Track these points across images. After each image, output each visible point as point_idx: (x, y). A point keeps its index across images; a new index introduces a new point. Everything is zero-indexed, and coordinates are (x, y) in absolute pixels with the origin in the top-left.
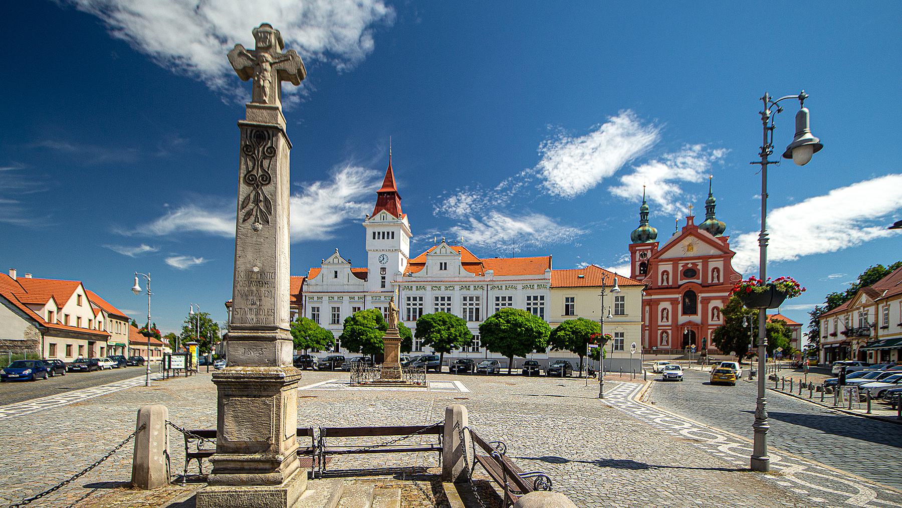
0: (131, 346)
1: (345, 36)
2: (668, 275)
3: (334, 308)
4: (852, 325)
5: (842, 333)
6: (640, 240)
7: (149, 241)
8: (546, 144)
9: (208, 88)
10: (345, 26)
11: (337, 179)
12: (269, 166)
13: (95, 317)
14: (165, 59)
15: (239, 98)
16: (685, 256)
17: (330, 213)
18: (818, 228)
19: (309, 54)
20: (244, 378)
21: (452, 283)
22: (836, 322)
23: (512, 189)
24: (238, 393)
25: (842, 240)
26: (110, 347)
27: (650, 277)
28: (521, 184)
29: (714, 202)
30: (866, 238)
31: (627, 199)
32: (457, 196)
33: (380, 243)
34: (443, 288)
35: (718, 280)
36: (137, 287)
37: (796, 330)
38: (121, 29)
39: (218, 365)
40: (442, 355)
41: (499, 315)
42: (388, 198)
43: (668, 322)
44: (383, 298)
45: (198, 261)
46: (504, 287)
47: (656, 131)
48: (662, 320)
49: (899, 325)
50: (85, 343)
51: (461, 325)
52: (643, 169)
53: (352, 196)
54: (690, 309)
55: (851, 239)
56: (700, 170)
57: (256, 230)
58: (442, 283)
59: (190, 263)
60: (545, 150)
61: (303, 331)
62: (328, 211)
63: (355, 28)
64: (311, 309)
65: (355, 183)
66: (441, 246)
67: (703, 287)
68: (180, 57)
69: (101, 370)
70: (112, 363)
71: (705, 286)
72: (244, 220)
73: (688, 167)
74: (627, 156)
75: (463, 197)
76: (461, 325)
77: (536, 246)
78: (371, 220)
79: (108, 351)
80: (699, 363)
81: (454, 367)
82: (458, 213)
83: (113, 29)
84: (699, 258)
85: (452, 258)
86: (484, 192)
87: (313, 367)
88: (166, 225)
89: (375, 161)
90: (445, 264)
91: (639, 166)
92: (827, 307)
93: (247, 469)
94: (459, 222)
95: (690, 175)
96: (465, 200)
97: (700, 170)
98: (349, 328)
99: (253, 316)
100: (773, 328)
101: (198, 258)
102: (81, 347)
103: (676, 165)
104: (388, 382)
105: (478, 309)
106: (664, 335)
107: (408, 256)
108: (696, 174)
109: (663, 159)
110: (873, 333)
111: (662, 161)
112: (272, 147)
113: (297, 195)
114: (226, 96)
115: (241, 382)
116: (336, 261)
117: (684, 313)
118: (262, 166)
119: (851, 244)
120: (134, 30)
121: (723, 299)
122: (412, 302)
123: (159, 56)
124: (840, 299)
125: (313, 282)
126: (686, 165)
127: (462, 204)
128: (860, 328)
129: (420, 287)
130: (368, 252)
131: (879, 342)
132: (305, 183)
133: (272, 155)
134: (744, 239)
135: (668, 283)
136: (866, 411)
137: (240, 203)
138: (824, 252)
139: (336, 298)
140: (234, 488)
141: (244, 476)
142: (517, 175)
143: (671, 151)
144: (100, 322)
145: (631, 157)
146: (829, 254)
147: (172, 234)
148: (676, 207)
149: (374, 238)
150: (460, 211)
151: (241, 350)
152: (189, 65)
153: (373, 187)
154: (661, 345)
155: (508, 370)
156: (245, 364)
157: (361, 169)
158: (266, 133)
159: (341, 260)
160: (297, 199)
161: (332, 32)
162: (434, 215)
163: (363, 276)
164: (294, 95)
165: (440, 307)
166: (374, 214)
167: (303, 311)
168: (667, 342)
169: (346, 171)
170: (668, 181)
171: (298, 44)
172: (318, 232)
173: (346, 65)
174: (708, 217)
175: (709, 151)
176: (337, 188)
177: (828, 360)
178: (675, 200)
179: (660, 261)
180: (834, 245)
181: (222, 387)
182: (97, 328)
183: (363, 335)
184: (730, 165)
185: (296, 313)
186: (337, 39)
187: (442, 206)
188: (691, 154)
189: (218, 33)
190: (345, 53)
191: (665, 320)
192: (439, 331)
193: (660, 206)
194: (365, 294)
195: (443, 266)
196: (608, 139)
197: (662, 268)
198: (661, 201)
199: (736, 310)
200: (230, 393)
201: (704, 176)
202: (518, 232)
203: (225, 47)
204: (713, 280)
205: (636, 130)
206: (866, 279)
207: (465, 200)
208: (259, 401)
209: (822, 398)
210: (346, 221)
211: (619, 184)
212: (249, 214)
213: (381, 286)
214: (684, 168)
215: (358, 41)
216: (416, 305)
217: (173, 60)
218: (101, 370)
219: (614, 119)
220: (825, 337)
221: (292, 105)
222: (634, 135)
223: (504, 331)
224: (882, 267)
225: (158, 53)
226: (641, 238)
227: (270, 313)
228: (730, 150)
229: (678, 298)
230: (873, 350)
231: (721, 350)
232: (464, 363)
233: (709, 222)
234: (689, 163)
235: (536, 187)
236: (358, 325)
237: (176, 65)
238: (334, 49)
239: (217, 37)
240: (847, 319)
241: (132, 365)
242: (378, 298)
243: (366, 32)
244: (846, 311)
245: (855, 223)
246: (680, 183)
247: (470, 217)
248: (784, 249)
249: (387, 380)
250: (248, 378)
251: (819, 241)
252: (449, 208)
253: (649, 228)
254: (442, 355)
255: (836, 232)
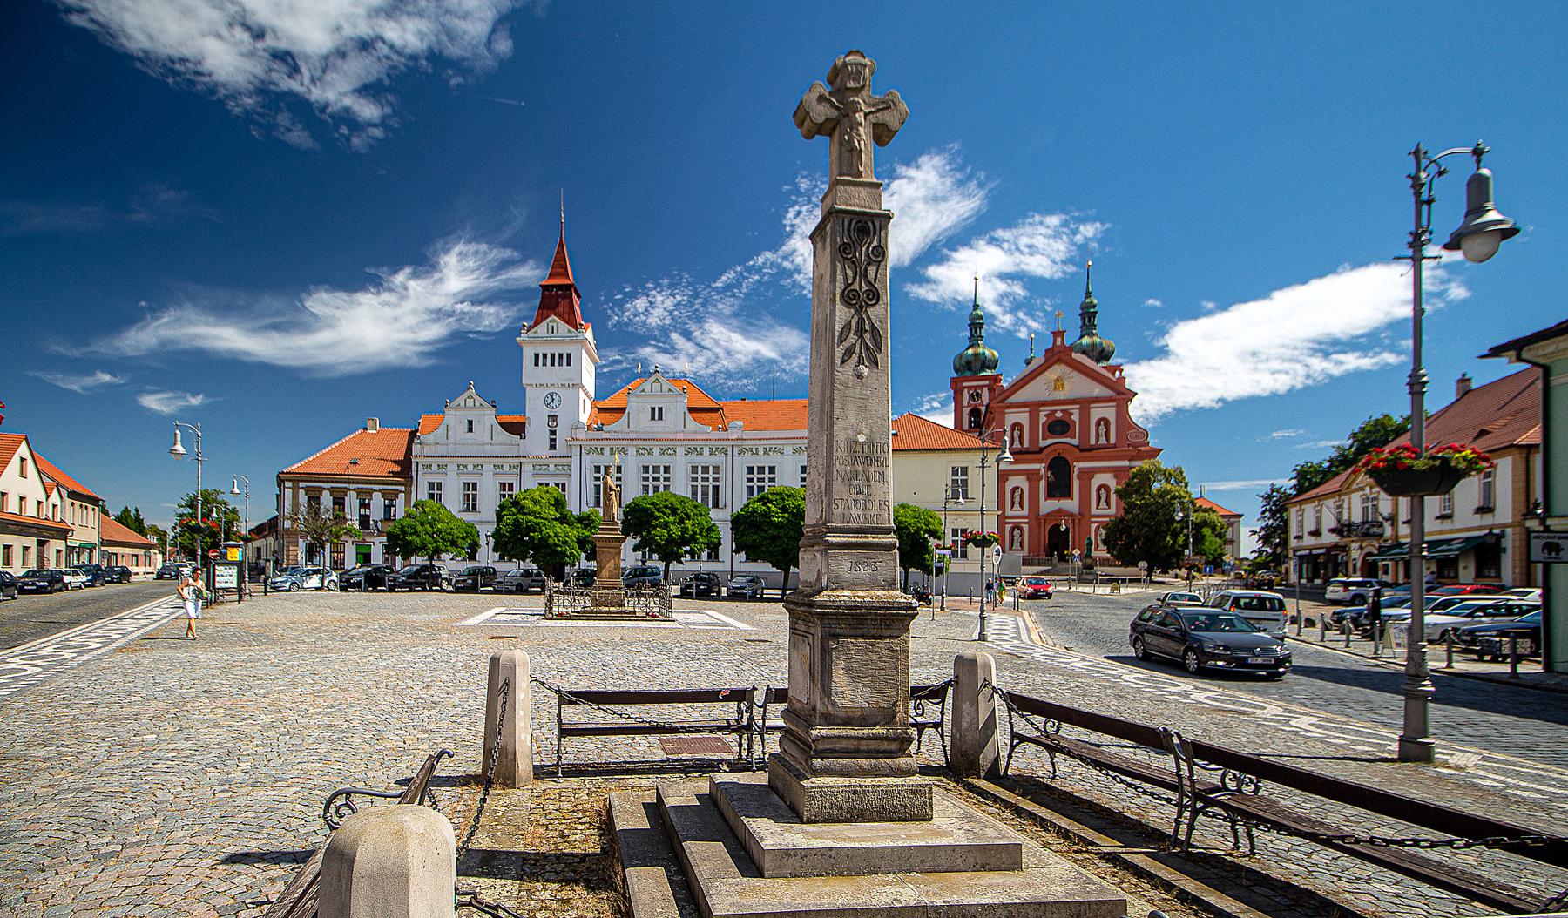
0: (103, 549)
1: (465, 32)
2: (1021, 429)
3: (467, 485)
4: (1350, 517)
5: (1332, 531)
6: (970, 370)
7: (111, 366)
8: (799, 213)
9: (228, 112)
10: (465, 16)
11: (442, 263)
12: (876, 276)
13: (48, 497)
14: (157, 62)
15: (282, 129)
16: (1051, 398)
17: (428, 321)
18: (1254, 354)
19: (403, 60)
20: (860, 608)
21: (671, 443)
22: (1320, 511)
23: (741, 285)
24: (848, 631)
25: (1296, 373)
26: (70, 549)
28: (757, 277)
29: (1094, 307)
30: (1336, 371)
31: (935, 304)
32: (648, 296)
33: (546, 373)
34: (656, 451)
35: (1108, 439)
36: (179, 448)
37: (1231, 525)
38: (83, 11)
39: (276, 583)
40: (667, 567)
41: (768, 498)
42: (560, 296)
44: (552, 468)
45: (196, 401)
46: (761, 451)
47: (982, 193)
48: (1012, 506)
49: (1437, 518)
50: (32, 542)
51: (701, 515)
52: (963, 254)
53: (467, 292)
54: (1059, 488)
55: (1311, 372)
56: (1057, 258)
57: (859, 376)
58: (655, 443)
59: (182, 403)
60: (796, 222)
61: (429, 523)
62: (425, 317)
63: (481, 19)
64: (427, 485)
65: (472, 271)
66: (653, 379)
67: (1082, 451)
68: (183, 60)
69: (67, 589)
70: (84, 578)
71: (1086, 450)
72: (843, 362)
73: (1038, 253)
74: (932, 236)
75: (659, 298)
76: (701, 515)
77: (783, 382)
78: (531, 333)
79: (68, 556)
80: (1081, 581)
81: (690, 586)
82: (650, 324)
83: (69, 10)
84: (1074, 402)
85: (671, 399)
86: (695, 289)
87: (441, 586)
88: (143, 338)
89: (507, 233)
90: (660, 409)
91: (956, 250)
92: (1295, 486)
93: (863, 752)
94: (652, 340)
95: (1041, 266)
96: (663, 302)
97: (1057, 258)
98: (509, 519)
99: (860, 512)
100: (1205, 521)
101: (195, 395)
102: (26, 549)
103: (1017, 249)
104: (609, 612)
105: (718, 487)
106: (1017, 532)
107: (592, 393)
108: (1050, 263)
109: (997, 240)
110: (1388, 531)
111: (994, 241)
112: (879, 246)
113: (372, 290)
114: (260, 126)
115: (857, 614)
116: (470, 402)
117: (1050, 495)
118: (866, 276)
119: (1310, 382)
120: (104, 12)
121: (1117, 472)
122: (755, 476)
123: (147, 57)
124: (1317, 472)
125: (430, 438)
126: (1034, 249)
127: (657, 310)
128: (1364, 523)
130: (525, 389)
131: (1401, 545)
132: (385, 268)
133: (879, 259)
134: (1132, 372)
135: (1021, 444)
136: (1444, 664)
137: (837, 334)
138: (1264, 394)
139: (470, 468)
140: (853, 781)
141: (863, 762)
142: (751, 263)
143: (1008, 225)
144: (54, 506)
145: (940, 234)
146: (1274, 396)
147: (153, 354)
148: (1018, 318)
149: (536, 364)
150: (653, 321)
151: (846, 565)
152: (201, 74)
153: (504, 277)
155: (780, 592)
156: (852, 586)
157: (484, 247)
159: (479, 401)
160: (370, 296)
161: (443, 25)
162: (610, 327)
163: (517, 429)
164: (375, 126)
165: (651, 483)
166: (536, 324)
167: (414, 488)
168: (1022, 544)
169: (457, 250)
170: (1003, 277)
171: (384, 42)
172: (407, 353)
173: (465, 79)
174: (1085, 332)
175: (1072, 226)
176: (441, 279)
177: (1305, 576)
178: (1015, 306)
179: (1008, 407)
180: (1281, 383)
181: (826, 621)
182: (51, 518)
183: (534, 531)
184: (1107, 250)
185: (349, 489)
186: (451, 35)
187: (623, 313)
188: (1043, 230)
189: (249, 22)
190: (463, 59)
191: (1017, 506)
192: (666, 526)
193: (992, 317)
194: (522, 460)
195: (657, 414)
196: (902, 205)
197: (1012, 417)
198: (993, 309)
199: (1142, 491)
200: (838, 631)
201: (1065, 268)
202: (753, 359)
203: (260, 45)
204: (1098, 440)
205: (948, 191)
206: (1363, 439)
207: (663, 302)
208: (881, 643)
209: (1348, 641)
210: (456, 335)
211: (924, 280)
212: (849, 352)
213: (548, 446)
214: (1031, 255)
215: (485, 40)
216: (707, 480)
217: (170, 65)
218: (67, 589)
219: (912, 172)
220: (1299, 537)
221: (371, 141)
222: (945, 199)
223: (776, 525)
224: (1390, 419)
225: (145, 52)
226: (970, 367)
227: (883, 507)
228: (1108, 225)
229: (1039, 470)
230: (1391, 560)
231: (1117, 557)
232: (703, 579)
233: (1086, 340)
234: (1041, 246)
235: (782, 283)
236: (525, 514)
237: (176, 73)
238: (446, 53)
239: (248, 28)
240: (1340, 507)
241: (112, 582)
242: (543, 467)
243: (500, 27)
244: (1338, 493)
245: (1316, 346)
246: (1026, 280)
247: (671, 331)
248: (1198, 388)
249: (607, 609)
250: (866, 608)
251: (1257, 377)
252: (635, 316)
253: (984, 350)
254: (667, 567)
255: (1284, 361)
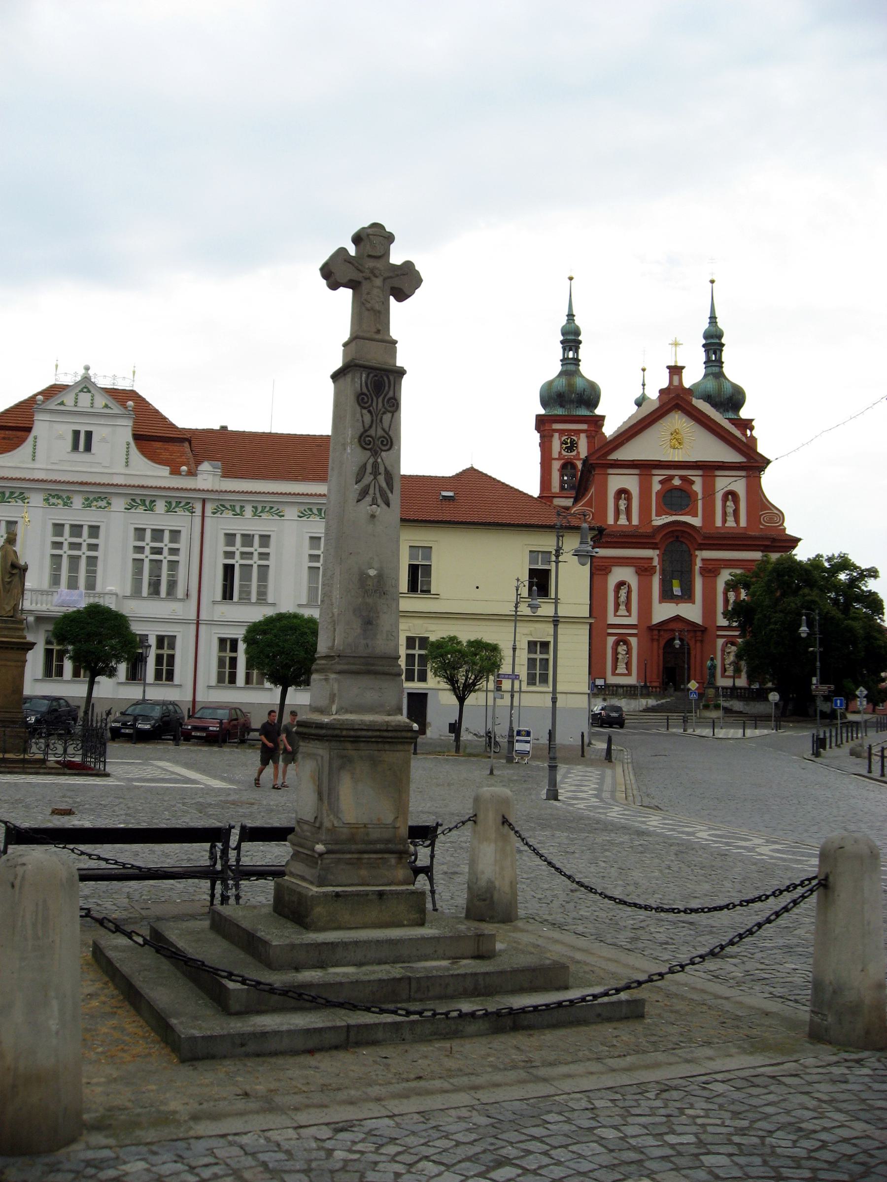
2: (629, 499)
27: (589, 504)
43: (630, 616)
106: (622, 649)
129: (12, 493)
154: (614, 674)
158: (385, 379)
168: (628, 665)
191: (622, 610)
204: (724, 521)
212: (364, 493)
229: (652, 559)
